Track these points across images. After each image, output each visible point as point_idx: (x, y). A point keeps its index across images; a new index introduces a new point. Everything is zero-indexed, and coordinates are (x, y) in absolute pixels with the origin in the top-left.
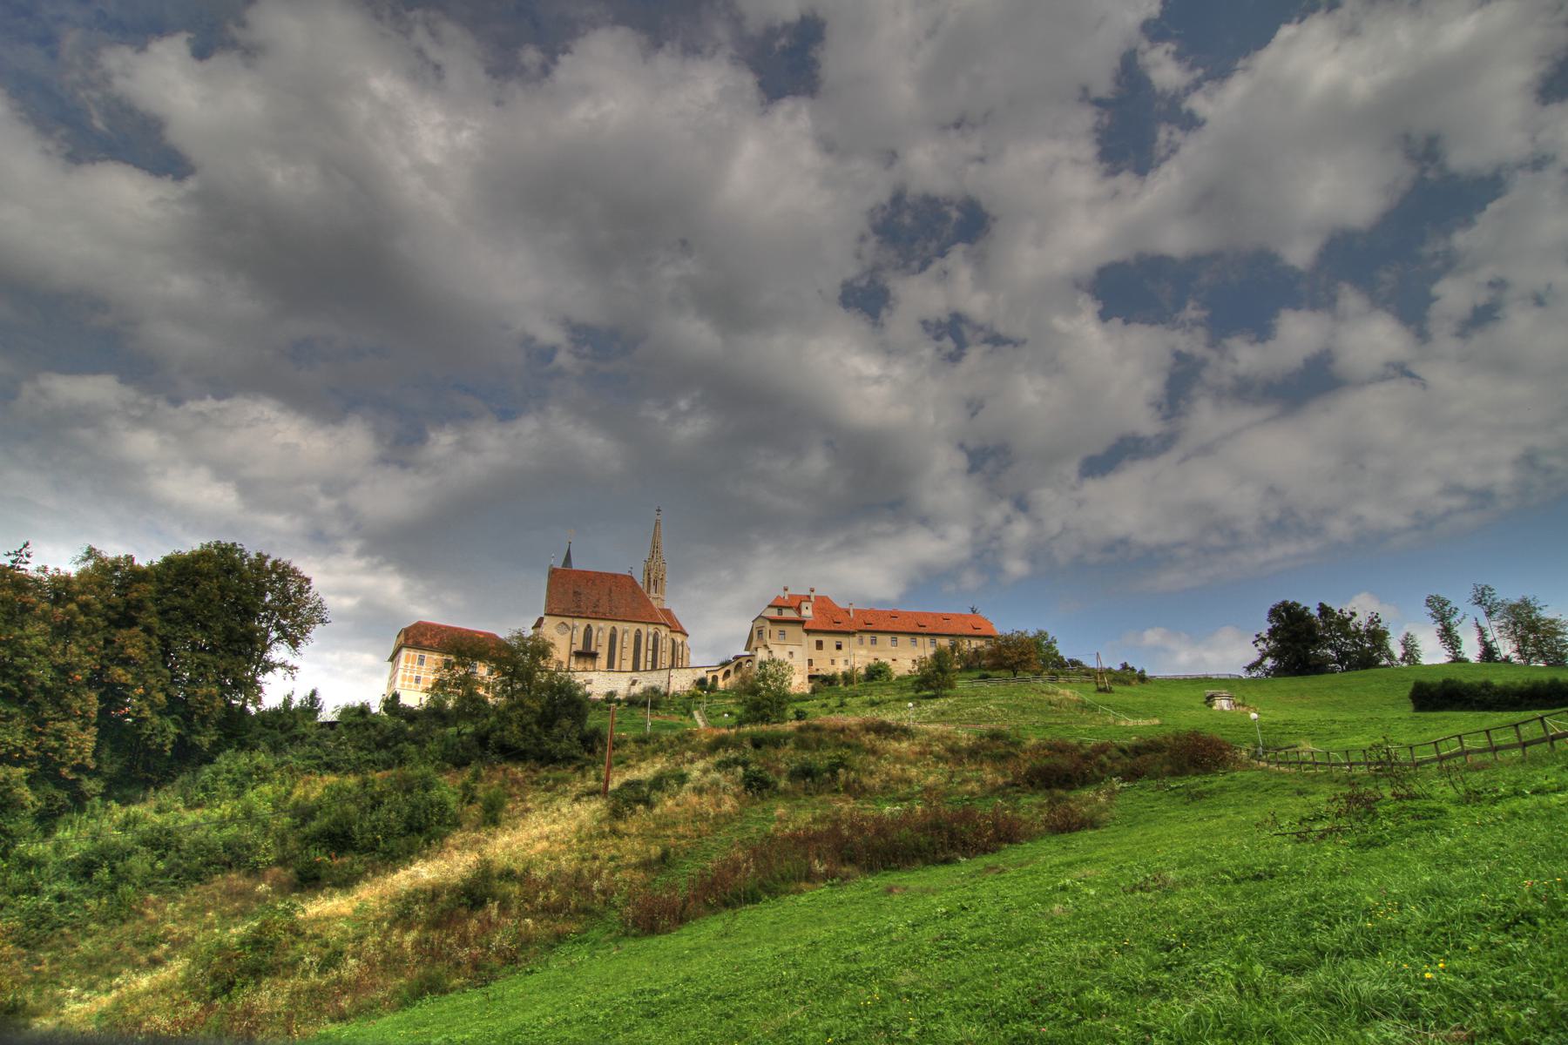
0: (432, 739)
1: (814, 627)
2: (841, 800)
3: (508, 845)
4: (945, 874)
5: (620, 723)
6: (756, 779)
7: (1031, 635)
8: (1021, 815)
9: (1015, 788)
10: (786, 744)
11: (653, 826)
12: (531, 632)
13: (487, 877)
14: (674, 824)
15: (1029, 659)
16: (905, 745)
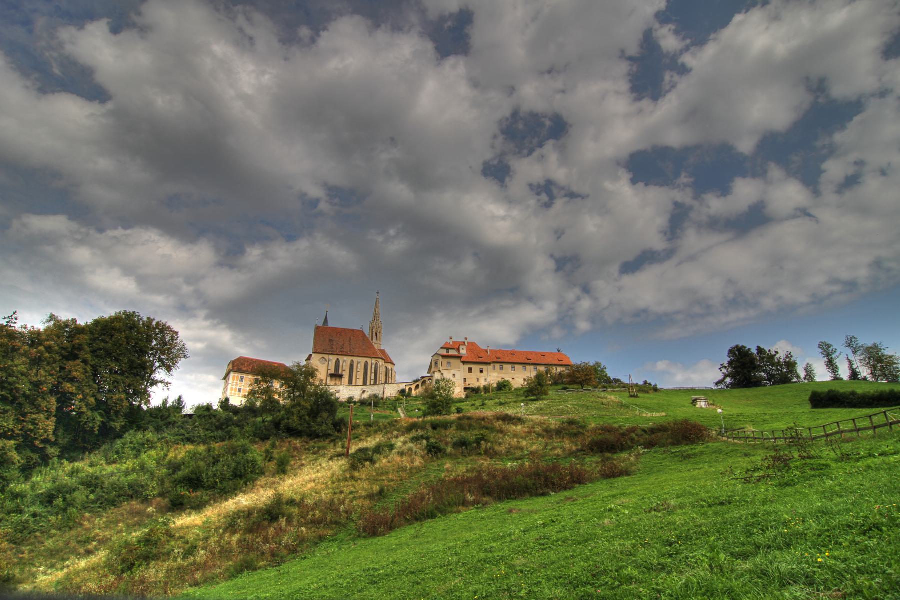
0: (248, 424)
1: (467, 360)
2: (483, 459)
3: (292, 485)
4: (542, 502)
5: (356, 415)
6: (434, 448)
7: (592, 365)
8: (586, 468)
9: (583, 453)
10: (451, 427)
11: (375, 474)
12: (305, 363)
13: (280, 504)
14: (387, 473)
15: (591, 378)
16: (519, 428)
